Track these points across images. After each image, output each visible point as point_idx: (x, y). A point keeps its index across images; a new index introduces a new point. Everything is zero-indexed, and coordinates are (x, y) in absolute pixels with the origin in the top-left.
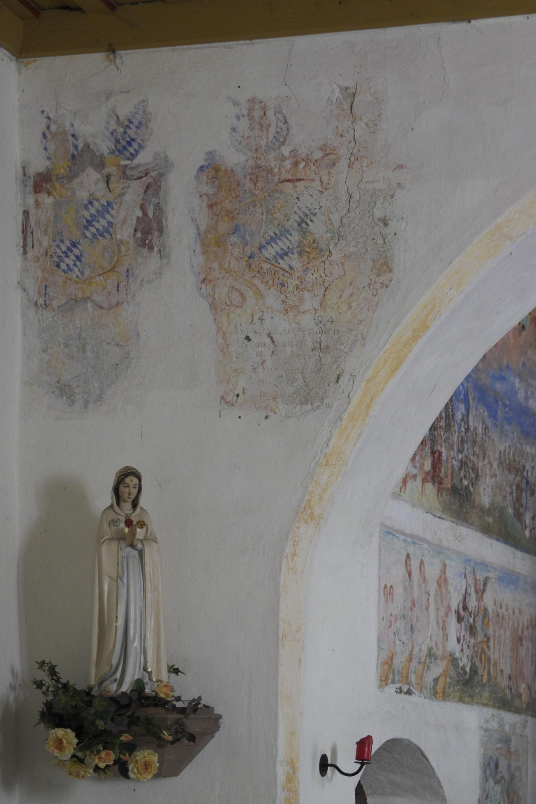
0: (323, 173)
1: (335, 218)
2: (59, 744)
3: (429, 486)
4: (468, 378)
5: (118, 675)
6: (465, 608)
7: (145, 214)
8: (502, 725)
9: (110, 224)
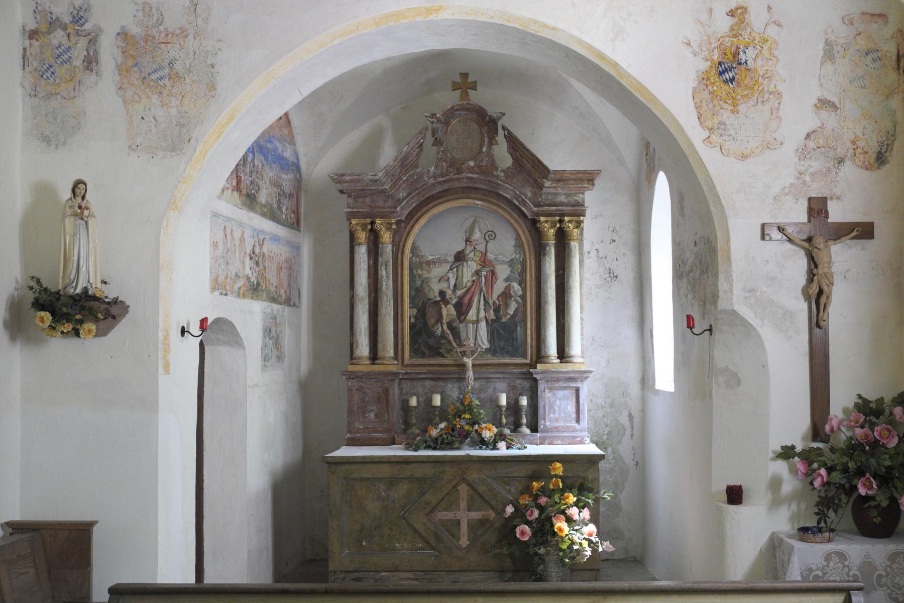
0: (181, 41)
1: (187, 62)
2: (42, 320)
3: (235, 193)
4: (255, 142)
5: (74, 284)
7: (88, 54)
8: (272, 310)
9: (70, 57)
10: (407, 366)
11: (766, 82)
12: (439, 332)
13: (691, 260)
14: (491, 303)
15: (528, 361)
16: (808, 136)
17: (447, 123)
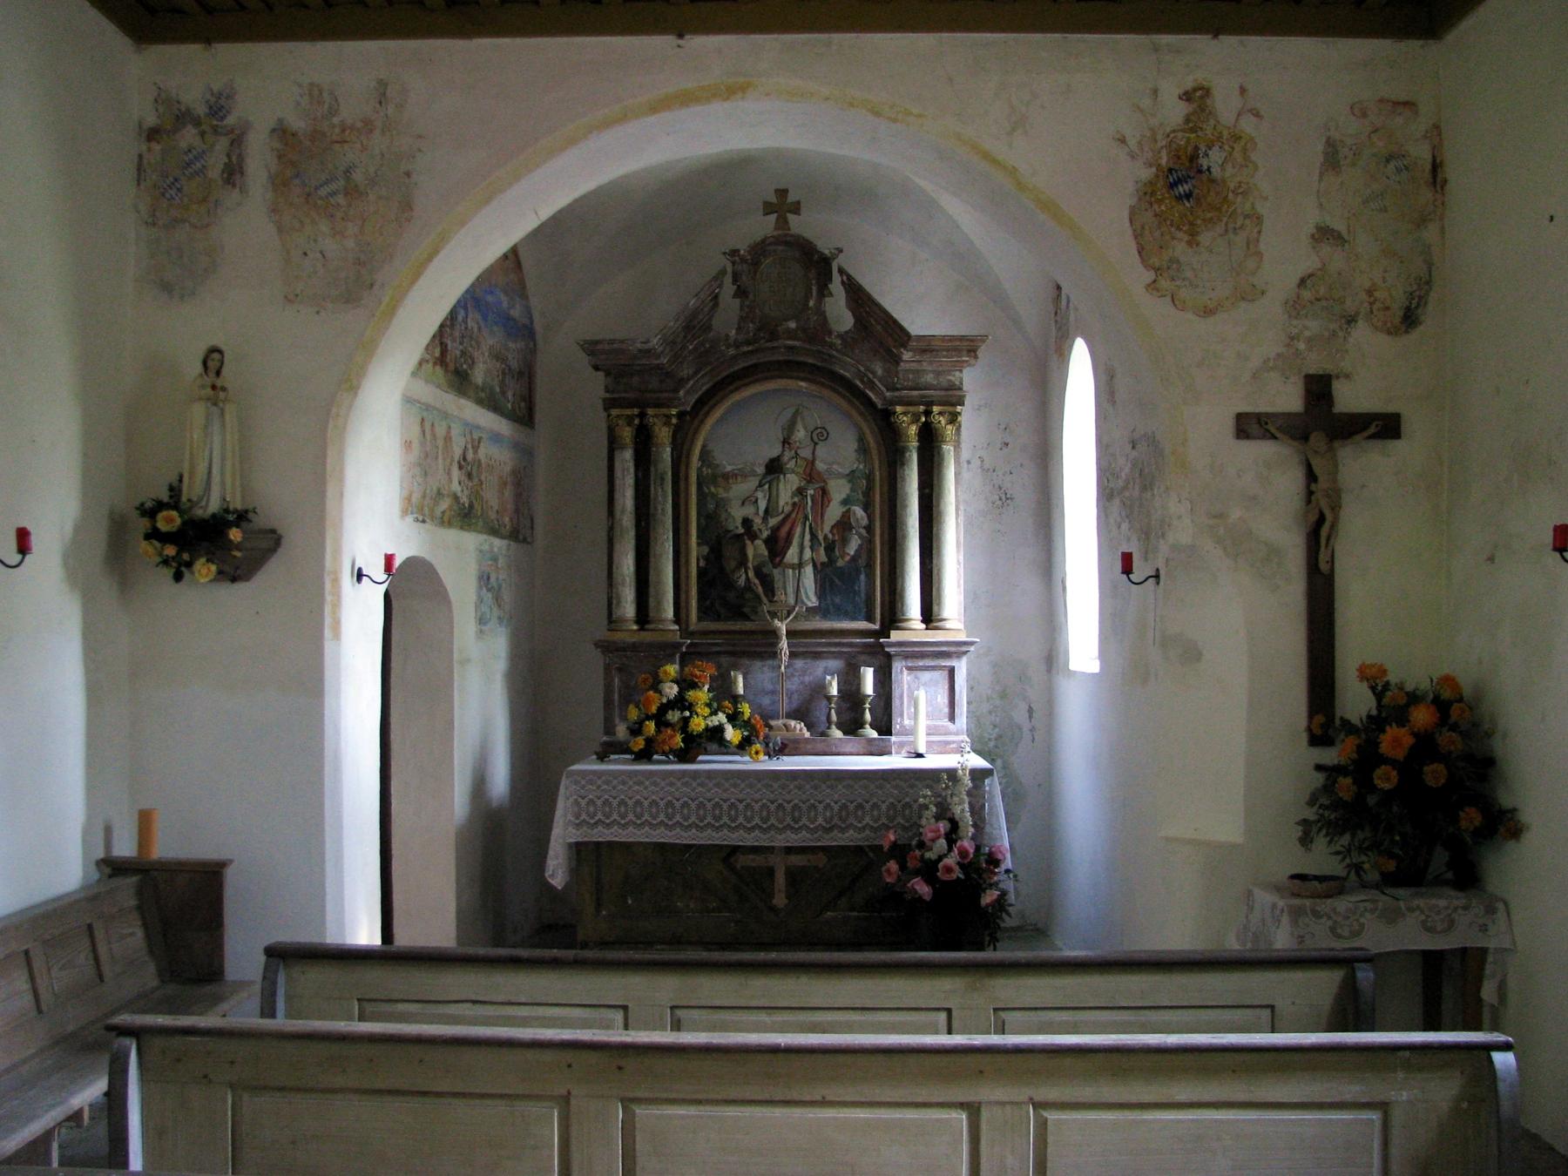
3: (438, 368)
4: (467, 291)
6: (465, 459)
10: (691, 634)
11: (1239, 199)
12: (742, 581)
13: (1127, 470)
14: (821, 538)
15: (877, 627)
16: (1302, 282)
17: (756, 264)
